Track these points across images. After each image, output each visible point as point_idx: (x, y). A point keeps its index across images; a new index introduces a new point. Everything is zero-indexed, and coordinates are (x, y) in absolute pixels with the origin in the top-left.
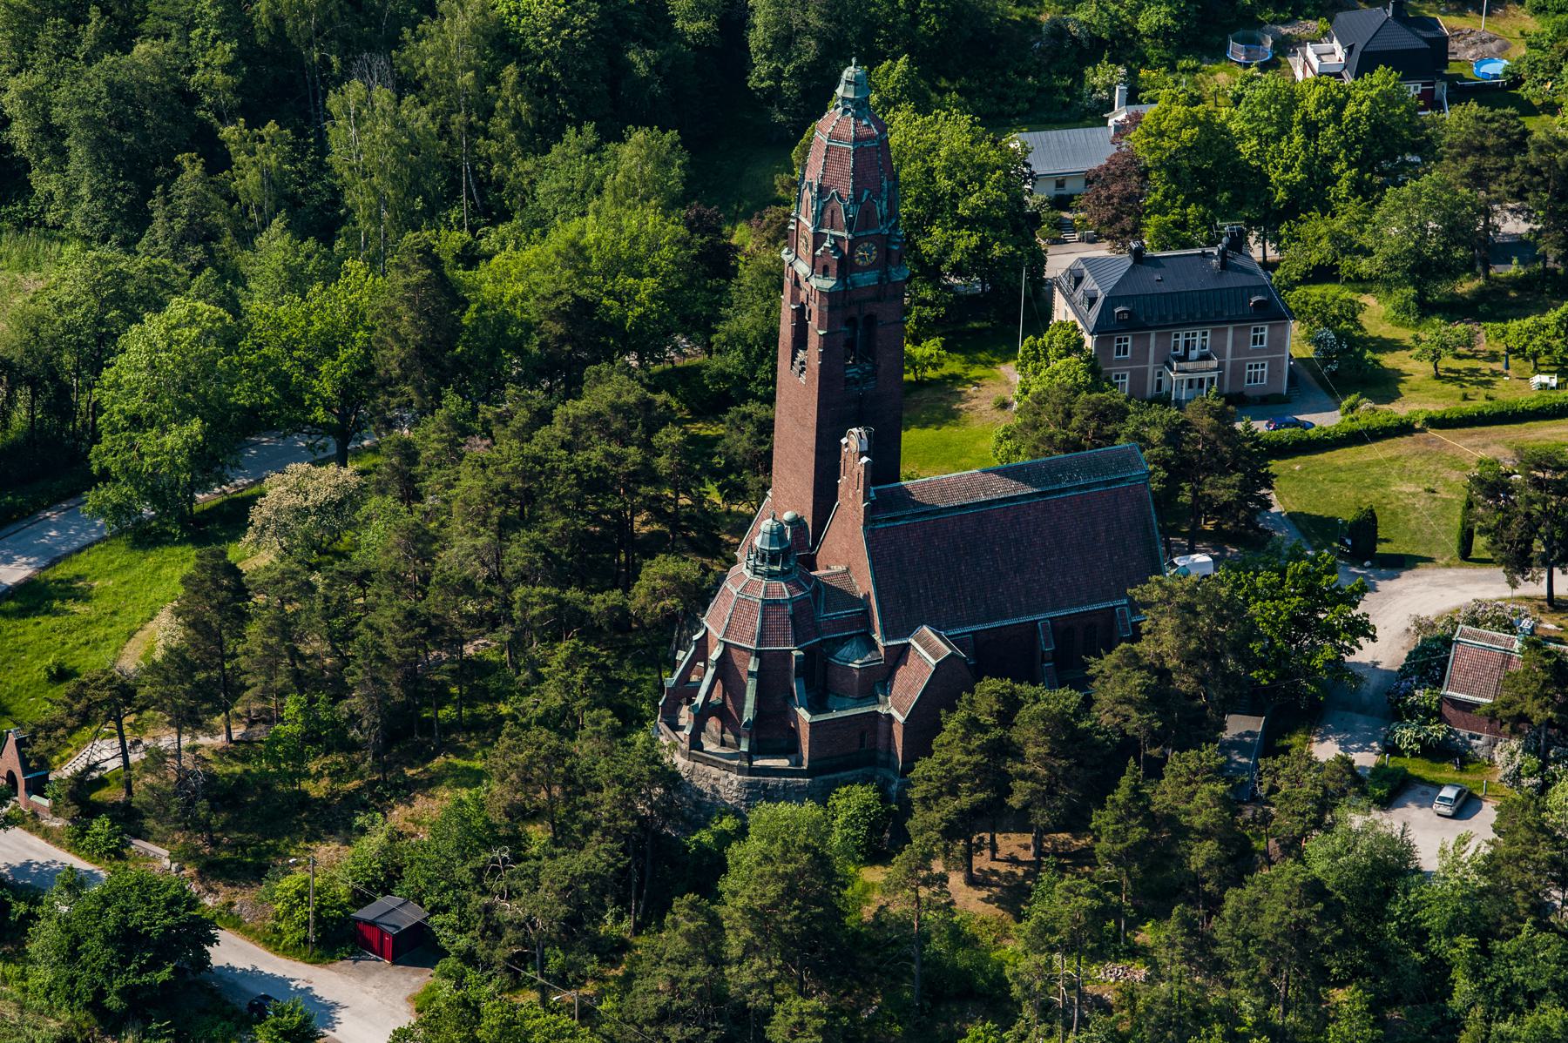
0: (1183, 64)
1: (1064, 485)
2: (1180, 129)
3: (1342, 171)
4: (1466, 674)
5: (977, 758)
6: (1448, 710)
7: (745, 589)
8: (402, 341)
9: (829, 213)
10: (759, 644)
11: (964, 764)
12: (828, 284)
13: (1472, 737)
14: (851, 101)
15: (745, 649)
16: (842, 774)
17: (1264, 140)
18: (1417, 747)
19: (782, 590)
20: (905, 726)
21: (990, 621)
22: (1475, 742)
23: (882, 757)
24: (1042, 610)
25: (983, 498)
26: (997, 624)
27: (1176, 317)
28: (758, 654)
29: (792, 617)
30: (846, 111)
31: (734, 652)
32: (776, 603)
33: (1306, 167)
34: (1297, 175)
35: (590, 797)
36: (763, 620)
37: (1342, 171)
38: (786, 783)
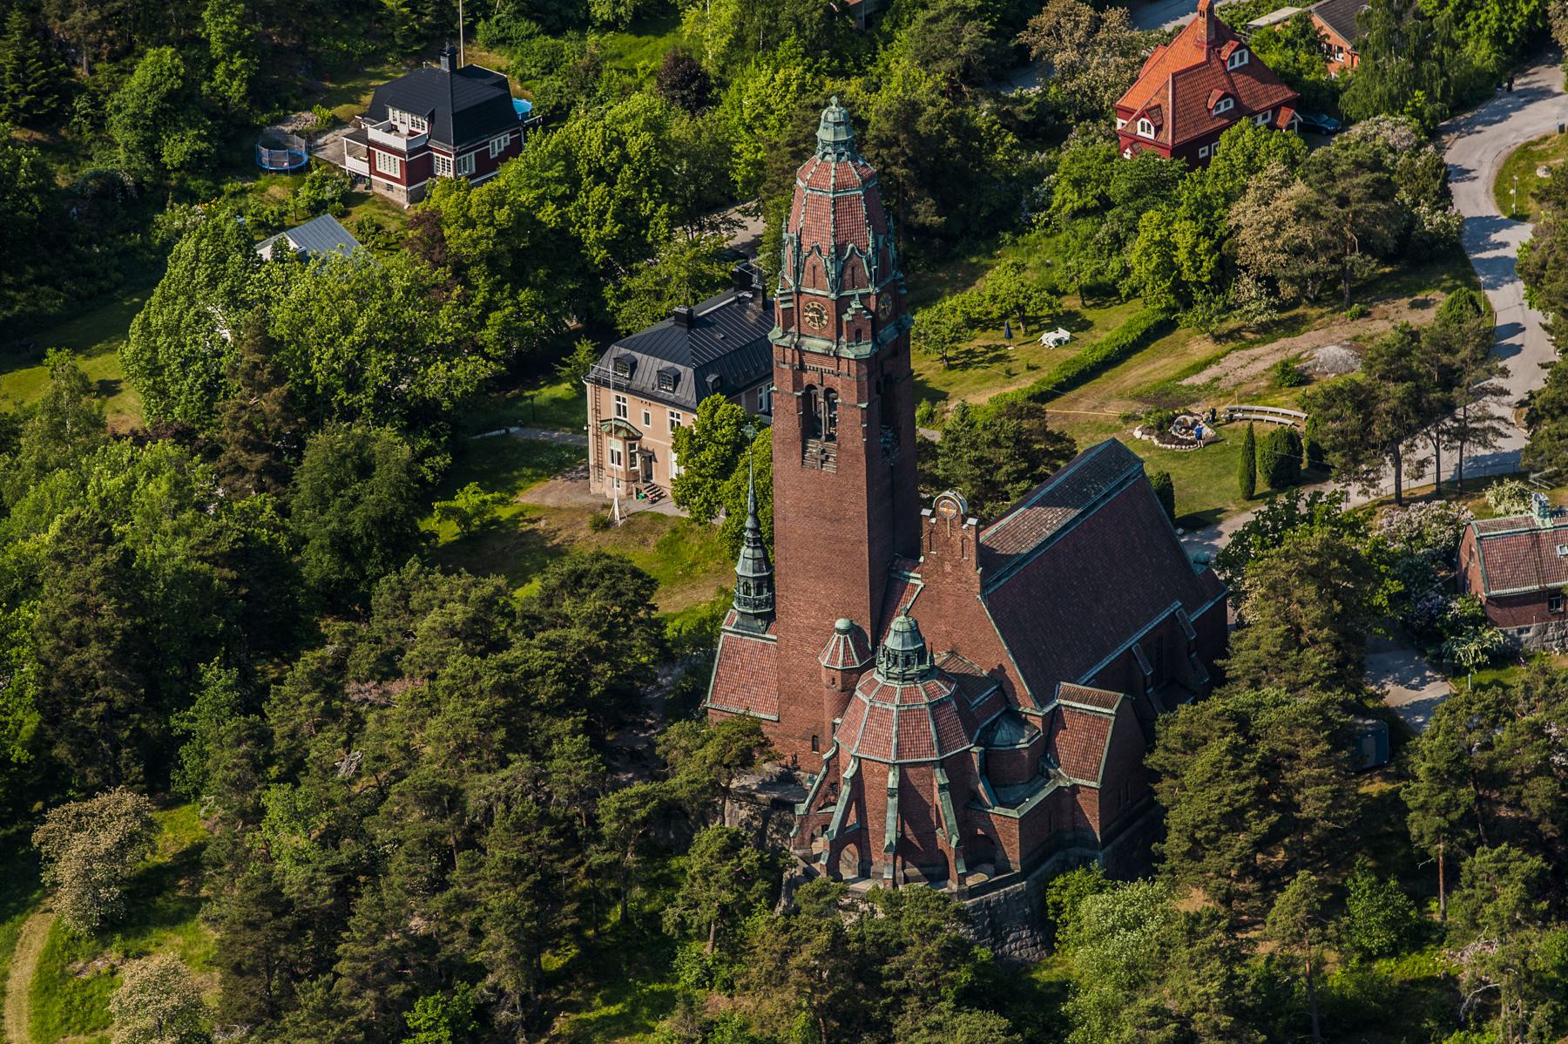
0: (228, 187)
1: (1095, 498)
2: (491, 212)
3: (653, 211)
4: (1502, 567)
5: (1252, 783)
6: (1494, 612)
7: (902, 699)
8: (104, 635)
9: (849, 271)
10: (941, 753)
11: (1243, 793)
12: (866, 349)
13: (1520, 631)
14: (844, 143)
15: (924, 764)
16: (1044, 867)
17: (562, 201)
18: (1483, 658)
19: (923, 694)
20: (1103, 792)
21: (1099, 659)
22: (1524, 636)
23: (1069, 836)
24: (1130, 635)
25: (1049, 533)
26: (1106, 662)
27: (757, 370)
28: (942, 764)
29: (958, 712)
30: (840, 155)
31: (910, 771)
32: (941, 703)
33: (618, 217)
34: (610, 228)
35: (895, 963)
36: (936, 725)
37: (653, 211)
38: (1006, 894)
